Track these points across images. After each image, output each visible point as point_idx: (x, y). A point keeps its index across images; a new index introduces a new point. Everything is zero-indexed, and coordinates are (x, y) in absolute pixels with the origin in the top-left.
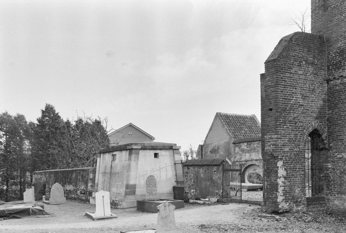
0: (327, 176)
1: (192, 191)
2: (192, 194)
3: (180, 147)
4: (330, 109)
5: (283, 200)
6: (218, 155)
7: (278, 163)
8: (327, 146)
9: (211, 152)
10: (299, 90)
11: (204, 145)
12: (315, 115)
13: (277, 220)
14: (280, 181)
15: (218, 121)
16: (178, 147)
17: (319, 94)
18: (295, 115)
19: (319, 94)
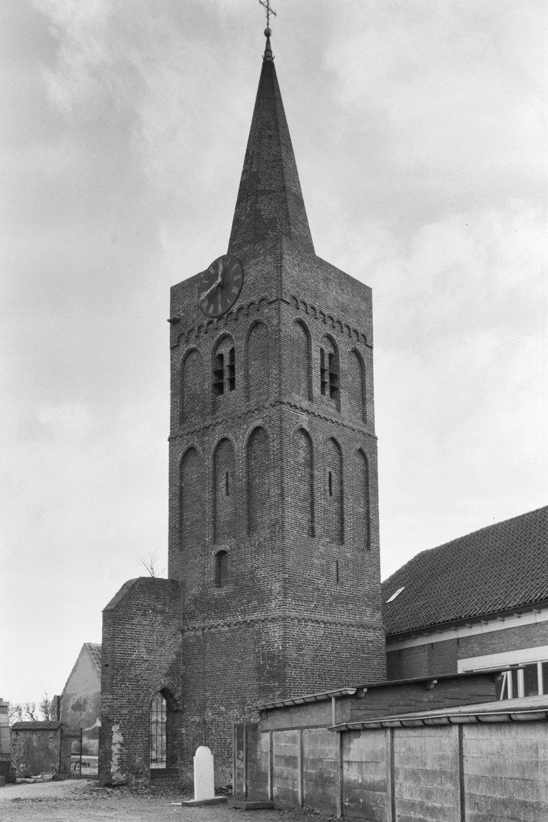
0: (181, 744)
1: (22, 765)
2: (22, 770)
3: (8, 703)
4: (184, 663)
5: (119, 770)
6: (84, 713)
7: (113, 727)
8: (181, 708)
9: (73, 708)
10: (142, 643)
11: (62, 696)
12: (164, 672)
13: (108, 793)
14: (115, 749)
15: (86, 657)
16: (5, 702)
17: (170, 646)
18: (137, 672)
19: (170, 646)
